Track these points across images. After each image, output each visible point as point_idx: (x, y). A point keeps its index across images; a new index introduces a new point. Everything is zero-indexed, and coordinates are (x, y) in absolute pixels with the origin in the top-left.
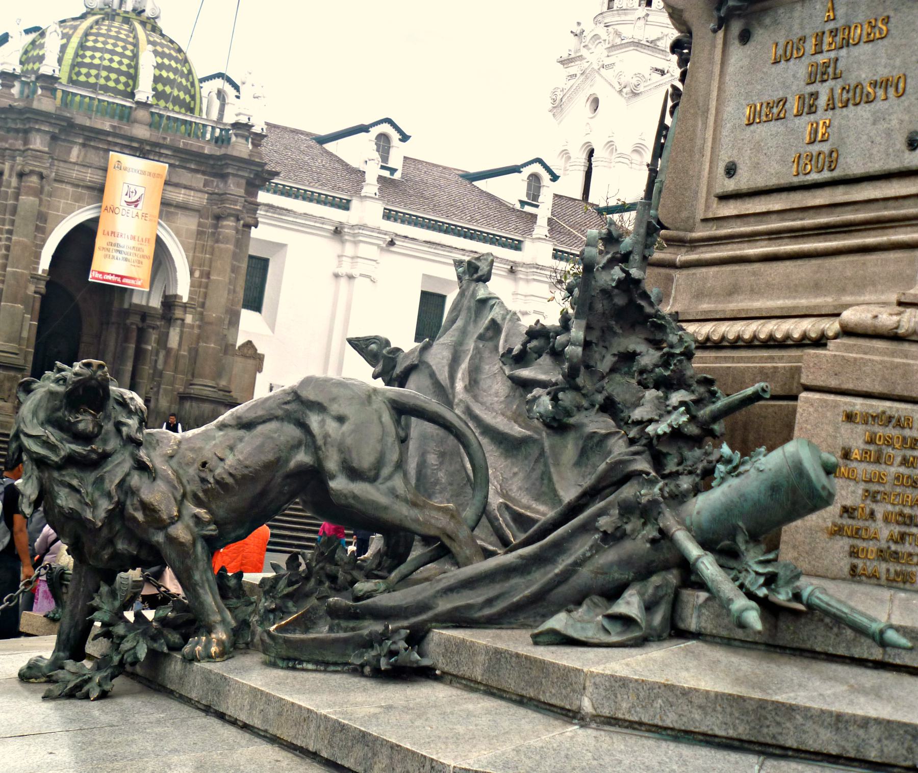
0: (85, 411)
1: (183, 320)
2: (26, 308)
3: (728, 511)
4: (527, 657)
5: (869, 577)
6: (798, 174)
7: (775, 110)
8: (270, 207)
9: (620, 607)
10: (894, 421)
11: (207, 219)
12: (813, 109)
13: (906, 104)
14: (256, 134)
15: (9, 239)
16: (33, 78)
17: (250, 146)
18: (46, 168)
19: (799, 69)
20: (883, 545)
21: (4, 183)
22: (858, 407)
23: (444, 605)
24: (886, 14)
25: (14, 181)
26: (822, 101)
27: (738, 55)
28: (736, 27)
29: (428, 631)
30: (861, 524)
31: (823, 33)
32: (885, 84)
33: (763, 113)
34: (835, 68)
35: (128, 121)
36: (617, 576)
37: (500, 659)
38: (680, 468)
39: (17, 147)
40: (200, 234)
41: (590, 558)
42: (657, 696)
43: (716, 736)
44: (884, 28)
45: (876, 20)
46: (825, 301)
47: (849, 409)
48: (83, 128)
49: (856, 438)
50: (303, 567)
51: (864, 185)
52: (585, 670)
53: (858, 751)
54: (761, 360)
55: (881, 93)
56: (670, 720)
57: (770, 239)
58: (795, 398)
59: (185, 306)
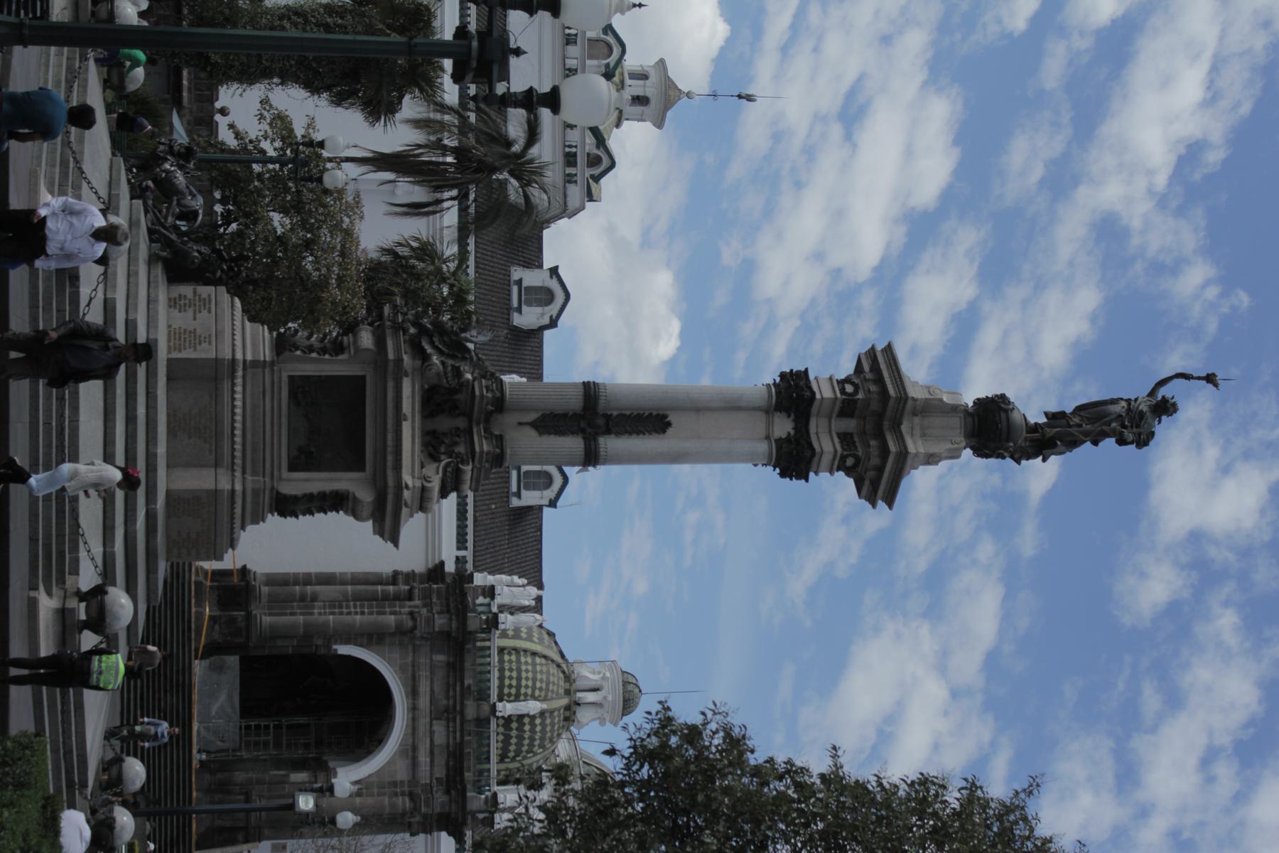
40: (394, 784)
48: (462, 661)
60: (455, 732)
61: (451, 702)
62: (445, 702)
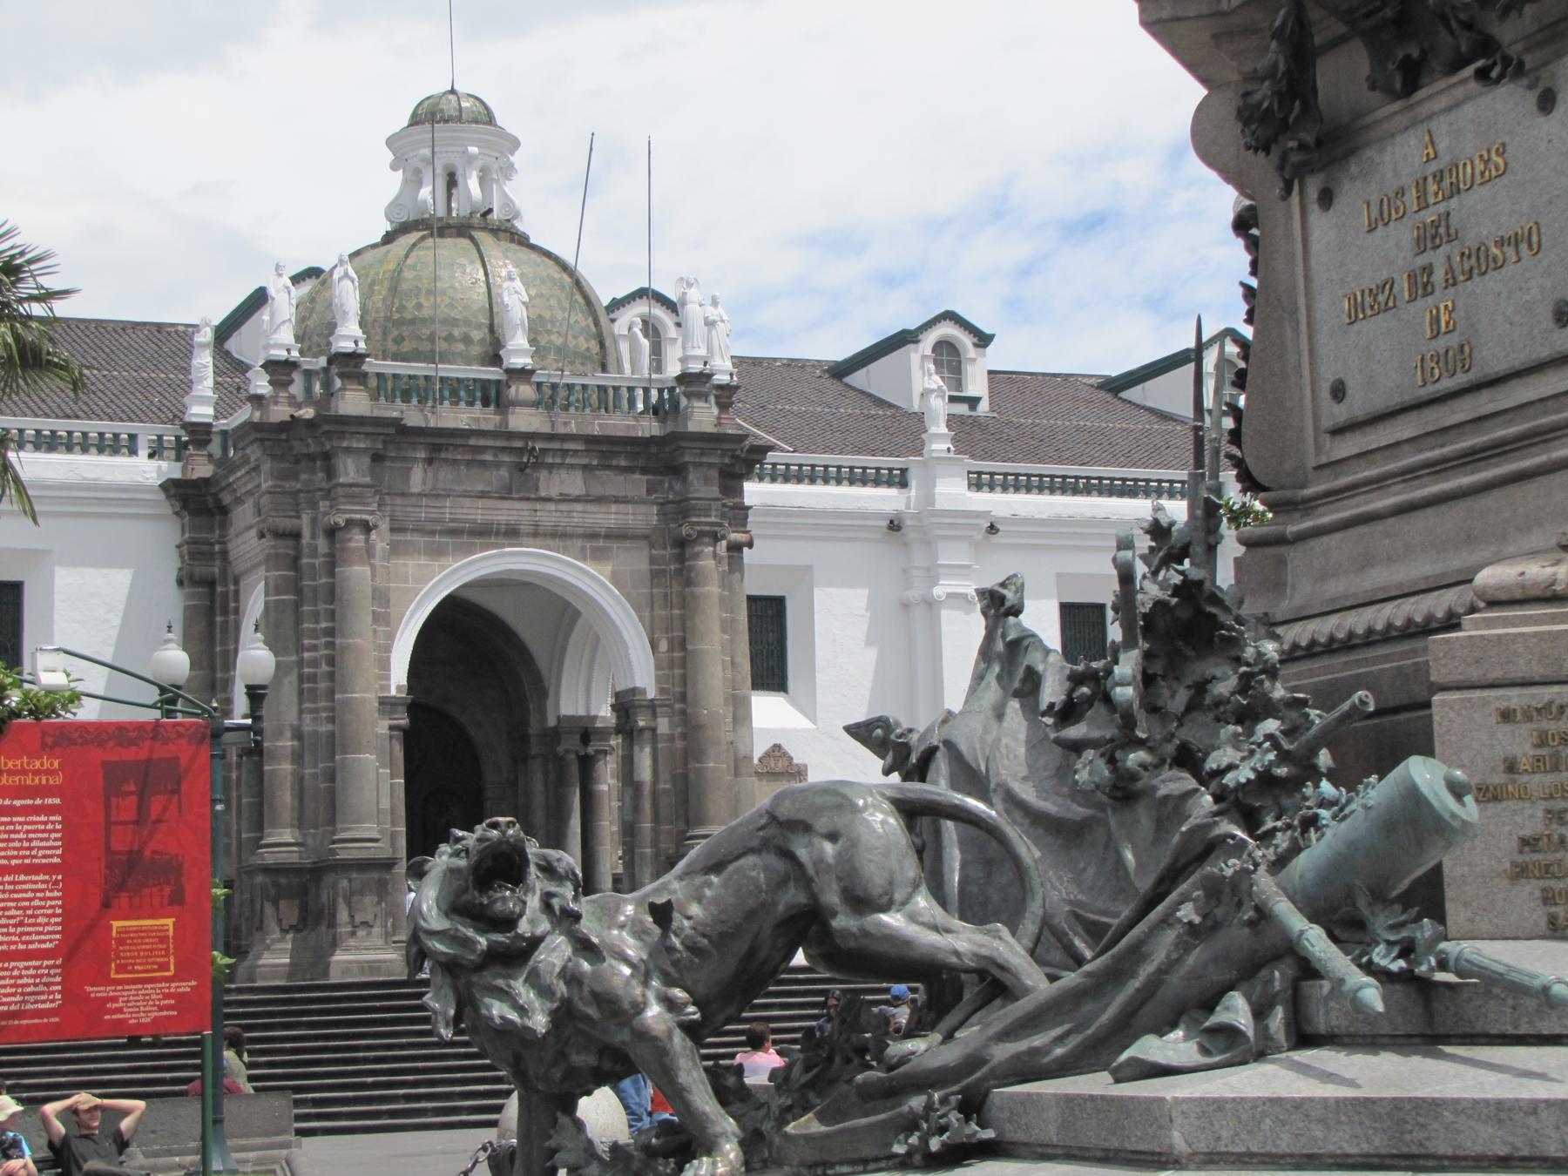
0: (500, 887)
1: (654, 730)
2: (378, 759)
3: (1339, 864)
4: (1103, 1098)
7: (1381, 298)
8: (771, 511)
9: (1220, 1017)
12: (1429, 289)
13: (1545, 263)
14: (720, 387)
15: (331, 645)
16: (322, 361)
17: (715, 411)
18: (372, 513)
19: (1402, 235)
21: (306, 551)
23: (1002, 1052)
24: (1500, 141)
25: (322, 545)
26: (1439, 275)
27: (1323, 226)
28: (1313, 186)
29: (987, 1093)
30: (1550, 857)
31: (1425, 179)
32: (1515, 241)
33: (1367, 306)
34: (1448, 227)
35: (498, 405)
36: (1215, 978)
38: (1279, 824)
39: (317, 485)
40: (655, 575)
42: (1264, 1115)
43: (1348, 1156)
44: (1500, 161)
45: (1489, 151)
46: (1456, 562)
47: (1503, 705)
49: (1519, 742)
51: (1513, 384)
52: (1168, 1097)
55: (1510, 252)
56: (1285, 1145)
57: (1404, 481)
58: (1427, 705)
59: (652, 707)
60: (564, 453)
62: (504, 473)
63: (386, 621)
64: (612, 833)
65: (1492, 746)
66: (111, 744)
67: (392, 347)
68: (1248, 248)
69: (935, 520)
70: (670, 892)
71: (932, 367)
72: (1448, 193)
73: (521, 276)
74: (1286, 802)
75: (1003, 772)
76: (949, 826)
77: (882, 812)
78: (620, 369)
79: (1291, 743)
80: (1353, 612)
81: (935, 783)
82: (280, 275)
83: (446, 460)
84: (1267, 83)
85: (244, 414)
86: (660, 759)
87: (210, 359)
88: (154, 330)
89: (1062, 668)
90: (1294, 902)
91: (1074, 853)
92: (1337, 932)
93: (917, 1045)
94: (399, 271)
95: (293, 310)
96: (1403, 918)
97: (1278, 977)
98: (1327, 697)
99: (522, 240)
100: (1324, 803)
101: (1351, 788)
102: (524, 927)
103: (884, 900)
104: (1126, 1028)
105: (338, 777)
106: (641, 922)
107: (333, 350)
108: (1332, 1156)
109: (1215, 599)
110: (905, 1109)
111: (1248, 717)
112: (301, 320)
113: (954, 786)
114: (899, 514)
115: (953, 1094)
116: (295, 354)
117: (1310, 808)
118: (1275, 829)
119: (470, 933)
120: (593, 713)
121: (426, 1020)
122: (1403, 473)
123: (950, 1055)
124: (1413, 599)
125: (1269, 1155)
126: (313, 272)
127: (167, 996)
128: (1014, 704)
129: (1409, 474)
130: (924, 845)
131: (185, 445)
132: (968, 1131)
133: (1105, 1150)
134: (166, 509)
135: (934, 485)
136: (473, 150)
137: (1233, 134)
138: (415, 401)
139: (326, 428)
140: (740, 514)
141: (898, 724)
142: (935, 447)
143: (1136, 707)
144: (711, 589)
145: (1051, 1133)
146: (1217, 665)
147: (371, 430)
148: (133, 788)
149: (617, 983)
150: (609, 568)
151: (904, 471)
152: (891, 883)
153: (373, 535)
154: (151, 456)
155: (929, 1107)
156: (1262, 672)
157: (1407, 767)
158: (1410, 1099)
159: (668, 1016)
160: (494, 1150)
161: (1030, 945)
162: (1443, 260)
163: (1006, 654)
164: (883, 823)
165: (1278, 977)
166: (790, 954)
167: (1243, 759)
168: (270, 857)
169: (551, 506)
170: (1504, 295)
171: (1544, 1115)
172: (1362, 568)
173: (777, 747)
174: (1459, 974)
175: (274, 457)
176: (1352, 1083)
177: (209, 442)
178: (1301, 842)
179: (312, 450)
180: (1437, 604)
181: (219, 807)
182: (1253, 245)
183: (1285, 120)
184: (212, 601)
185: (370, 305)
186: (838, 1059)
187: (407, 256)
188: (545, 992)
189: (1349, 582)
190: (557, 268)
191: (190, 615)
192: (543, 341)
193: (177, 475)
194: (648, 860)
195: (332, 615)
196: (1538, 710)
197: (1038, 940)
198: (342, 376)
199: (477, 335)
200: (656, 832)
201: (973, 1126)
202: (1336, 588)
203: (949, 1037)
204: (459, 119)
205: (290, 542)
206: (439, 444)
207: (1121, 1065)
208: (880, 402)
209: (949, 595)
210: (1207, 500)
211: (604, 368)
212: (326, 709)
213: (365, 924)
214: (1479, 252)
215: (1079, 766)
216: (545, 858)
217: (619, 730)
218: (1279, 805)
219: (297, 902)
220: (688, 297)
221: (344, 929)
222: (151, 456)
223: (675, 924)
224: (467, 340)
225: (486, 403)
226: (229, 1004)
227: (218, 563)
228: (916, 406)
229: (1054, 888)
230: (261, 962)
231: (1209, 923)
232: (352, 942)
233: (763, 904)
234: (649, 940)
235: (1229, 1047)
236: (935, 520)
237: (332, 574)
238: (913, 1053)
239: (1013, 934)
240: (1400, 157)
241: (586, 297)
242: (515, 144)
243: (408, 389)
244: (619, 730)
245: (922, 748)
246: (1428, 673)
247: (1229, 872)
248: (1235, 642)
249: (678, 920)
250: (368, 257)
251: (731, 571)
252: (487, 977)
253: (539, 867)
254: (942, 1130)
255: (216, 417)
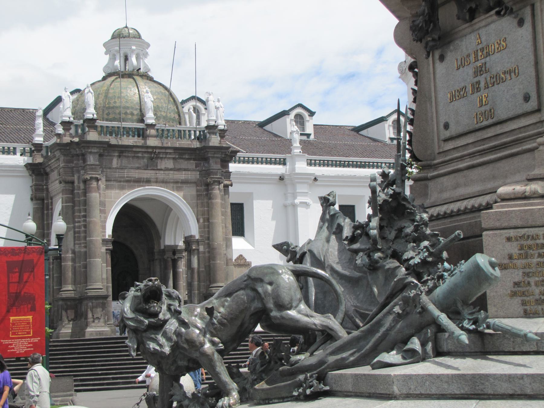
0: (153, 302)
1: (198, 250)
2: (102, 260)
3: (451, 292)
4: (368, 375)
5: (534, 314)
6: (477, 123)
7: (462, 93)
8: (239, 174)
9: (409, 346)
10: (531, 237)
11: (201, 186)
12: (479, 89)
13: (520, 80)
14: (221, 130)
15: (85, 221)
16: (81, 122)
17: (219, 139)
18: (99, 174)
19: (469, 70)
20: (537, 297)
21: (76, 188)
22: (512, 234)
23: (332, 359)
24: (504, 37)
25: (82, 186)
26: (482, 85)
27: (441, 68)
28: (437, 54)
29: (326, 373)
30: (524, 289)
31: (477, 51)
32: (510, 72)
33: (456, 96)
35: (143, 137)
37: (357, 379)
41: (394, 326)
42: (426, 380)
44: (504, 44)
45: (500, 41)
46: (489, 186)
47: (507, 235)
49: (513, 248)
50: (267, 357)
51: (509, 123)
52: (392, 374)
53: (522, 390)
54: (470, 219)
55: (508, 76)
56: (434, 391)
57: (470, 157)
59: (198, 242)
60: (166, 153)
61: (146, 155)
63: (104, 212)
64: (184, 286)
65: (504, 250)
66: (10, 255)
67: (105, 116)
68: (414, 76)
69: (295, 176)
70: (213, 304)
71: (294, 123)
72: (485, 55)
73: (151, 92)
74: (431, 270)
75: (330, 260)
76: (311, 279)
77: (288, 275)
78: (186, 124)
79: (433, 249)
80: (453, 204)
81: (306, 264)
82: (66, 91)
83: (125, 156)
84: (421, 17)
85: (54, 140)
86: (200, 259)
87: (42, 121)
88: (22, 111)
89: (350, 224)
90: (434, 304)
91: (356, 289)
92: (450, 316)
93: (301, 357)
94: (108, 90)
95: (71, 103)
96: (474, 310)
97: (430, 332)
98: (445, 233)
99: (151, 79)
100: (445, 270)
101: (455, 265)
102: (161, 316)
103: (289, 306)
104: (376, 350)
105: (88, 267)
106: (203, 314)
107: (85, 118)
108: (450, 394)
109: (405, 199)
110: (297, 379)
111: (417, 240)
112: (74, 107)
113: (312, 265)
114: (283, 174)
115: (314, 374)
116: (72, 119)
117: (440, 272)
118: (428, 280)
119: (142, 318)
120: (177, 244)
121: (127, 351)
122: (470, 154)
123: (313, 360)
124: (474, 199)
125: (428, 394)
126: (78, 91)
127: (30, 343)
128: (333, 237)
129: (472, 155)
130: (303, 286)
131: (33, 151)
132: (320, 387)
133: (370, 393)
134: (26, 173)
135: (295, 164)
136: (134, 48)
137: (409, 35)
138: (114, 135)
139: (83, 145)
140: (228, 175)
141: (292, 244)
142: (295, 151)
143: (378, 237)
144: (218, 201)
145: (350, 388)
146: (406, 222)
147: (98, 145)
148: (17, 270)
149: (195, 336)
150: (182, 194)
151: (285, 159)
152: (291, 300)
153: (100, 182)
154: (21, 155)
155: (306, 379)
156: (422, 224)
157: (475, 257)
158: (478, 374)
159: (213, 347)
160: (147, 396)
161: (341, 321)
162: (484, 79)
163: (329, 221)
164: (288, 279)
165: (430, 332)
166: (255, 326)
167: (416, 255)
168: (64, 295)
169: (162, 172)
170: (506, 91)
171: (526, 380)
172: (455, 188)
173: (241, 256)
174: (494, 330)
175: (64, 155)
176: (457, 369)
177: (42, 150)
178: (437, 284)
179: (78, 152)
180: (483, 200)
181: (47, 277)
182: (416, 75)
183: (427, 30)
184: (43, 205)
185: (98, 102)
186: (272, 363)
187: (111, 85)
188: (169, 339)
189: (451, 192)
190: (163, 89)
191: (35, 211)
192: (159, 115)
193: (31, 162)
194: (196, 295)
195: (85, 210)
196: (520, 237)
197: (343, 321)
198: (88, 127)
199: (135, 112)
200: (199, 286)
201: (322, 385)
202: (446, 195)
203: (312, 354)
204: (129, 37)
205: (70, 185)
206: (123, 150)
207: (374, 363)
208: (276, 136)
209: (301, 203)
210: (402, 164)
211: (180, 124)
212: (83, 243)
213: (98, 318)
214: (497, 76)
215: (357, 258)
216: (168, 292)
217: (186, 250)
218: (429, 271)
219: (73, 311)
220: (209, 99)
221: (90, 320)
222: (21, 155)
223: (215, 315)
224: (132, 114)
225: (139, 136)
226: (50, 346)
227: (45, 192)
228: (289, 137)
229: (348, 301)
230: (61, 332)
231: (405, 313)
232: (93, 324)
233: (246, 308)
234: (206, 321)
235: (412, 357)
236: (295, 176)
237: (85, 196)
238: (300, 360)
239: (335, 318)
240: (468, 43)
241: (174, 99)
242: (148, 45)
243: (112, 131)
244: (186, 250)
245: (301, 252)
246: (481, 225)
247: (412, 295)
248: (413, 214)
249: (216, 314)
250: (97, 85)
251: (225, 194)
252: (148, 334)
253: (167, 295)
254: (310, 387)
255: (44, 142)
